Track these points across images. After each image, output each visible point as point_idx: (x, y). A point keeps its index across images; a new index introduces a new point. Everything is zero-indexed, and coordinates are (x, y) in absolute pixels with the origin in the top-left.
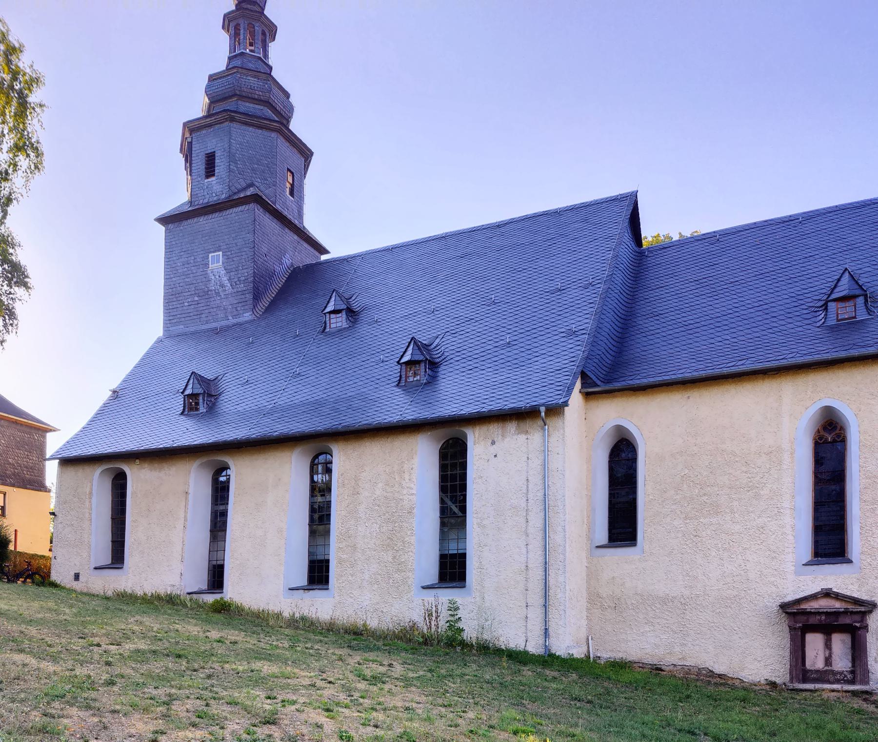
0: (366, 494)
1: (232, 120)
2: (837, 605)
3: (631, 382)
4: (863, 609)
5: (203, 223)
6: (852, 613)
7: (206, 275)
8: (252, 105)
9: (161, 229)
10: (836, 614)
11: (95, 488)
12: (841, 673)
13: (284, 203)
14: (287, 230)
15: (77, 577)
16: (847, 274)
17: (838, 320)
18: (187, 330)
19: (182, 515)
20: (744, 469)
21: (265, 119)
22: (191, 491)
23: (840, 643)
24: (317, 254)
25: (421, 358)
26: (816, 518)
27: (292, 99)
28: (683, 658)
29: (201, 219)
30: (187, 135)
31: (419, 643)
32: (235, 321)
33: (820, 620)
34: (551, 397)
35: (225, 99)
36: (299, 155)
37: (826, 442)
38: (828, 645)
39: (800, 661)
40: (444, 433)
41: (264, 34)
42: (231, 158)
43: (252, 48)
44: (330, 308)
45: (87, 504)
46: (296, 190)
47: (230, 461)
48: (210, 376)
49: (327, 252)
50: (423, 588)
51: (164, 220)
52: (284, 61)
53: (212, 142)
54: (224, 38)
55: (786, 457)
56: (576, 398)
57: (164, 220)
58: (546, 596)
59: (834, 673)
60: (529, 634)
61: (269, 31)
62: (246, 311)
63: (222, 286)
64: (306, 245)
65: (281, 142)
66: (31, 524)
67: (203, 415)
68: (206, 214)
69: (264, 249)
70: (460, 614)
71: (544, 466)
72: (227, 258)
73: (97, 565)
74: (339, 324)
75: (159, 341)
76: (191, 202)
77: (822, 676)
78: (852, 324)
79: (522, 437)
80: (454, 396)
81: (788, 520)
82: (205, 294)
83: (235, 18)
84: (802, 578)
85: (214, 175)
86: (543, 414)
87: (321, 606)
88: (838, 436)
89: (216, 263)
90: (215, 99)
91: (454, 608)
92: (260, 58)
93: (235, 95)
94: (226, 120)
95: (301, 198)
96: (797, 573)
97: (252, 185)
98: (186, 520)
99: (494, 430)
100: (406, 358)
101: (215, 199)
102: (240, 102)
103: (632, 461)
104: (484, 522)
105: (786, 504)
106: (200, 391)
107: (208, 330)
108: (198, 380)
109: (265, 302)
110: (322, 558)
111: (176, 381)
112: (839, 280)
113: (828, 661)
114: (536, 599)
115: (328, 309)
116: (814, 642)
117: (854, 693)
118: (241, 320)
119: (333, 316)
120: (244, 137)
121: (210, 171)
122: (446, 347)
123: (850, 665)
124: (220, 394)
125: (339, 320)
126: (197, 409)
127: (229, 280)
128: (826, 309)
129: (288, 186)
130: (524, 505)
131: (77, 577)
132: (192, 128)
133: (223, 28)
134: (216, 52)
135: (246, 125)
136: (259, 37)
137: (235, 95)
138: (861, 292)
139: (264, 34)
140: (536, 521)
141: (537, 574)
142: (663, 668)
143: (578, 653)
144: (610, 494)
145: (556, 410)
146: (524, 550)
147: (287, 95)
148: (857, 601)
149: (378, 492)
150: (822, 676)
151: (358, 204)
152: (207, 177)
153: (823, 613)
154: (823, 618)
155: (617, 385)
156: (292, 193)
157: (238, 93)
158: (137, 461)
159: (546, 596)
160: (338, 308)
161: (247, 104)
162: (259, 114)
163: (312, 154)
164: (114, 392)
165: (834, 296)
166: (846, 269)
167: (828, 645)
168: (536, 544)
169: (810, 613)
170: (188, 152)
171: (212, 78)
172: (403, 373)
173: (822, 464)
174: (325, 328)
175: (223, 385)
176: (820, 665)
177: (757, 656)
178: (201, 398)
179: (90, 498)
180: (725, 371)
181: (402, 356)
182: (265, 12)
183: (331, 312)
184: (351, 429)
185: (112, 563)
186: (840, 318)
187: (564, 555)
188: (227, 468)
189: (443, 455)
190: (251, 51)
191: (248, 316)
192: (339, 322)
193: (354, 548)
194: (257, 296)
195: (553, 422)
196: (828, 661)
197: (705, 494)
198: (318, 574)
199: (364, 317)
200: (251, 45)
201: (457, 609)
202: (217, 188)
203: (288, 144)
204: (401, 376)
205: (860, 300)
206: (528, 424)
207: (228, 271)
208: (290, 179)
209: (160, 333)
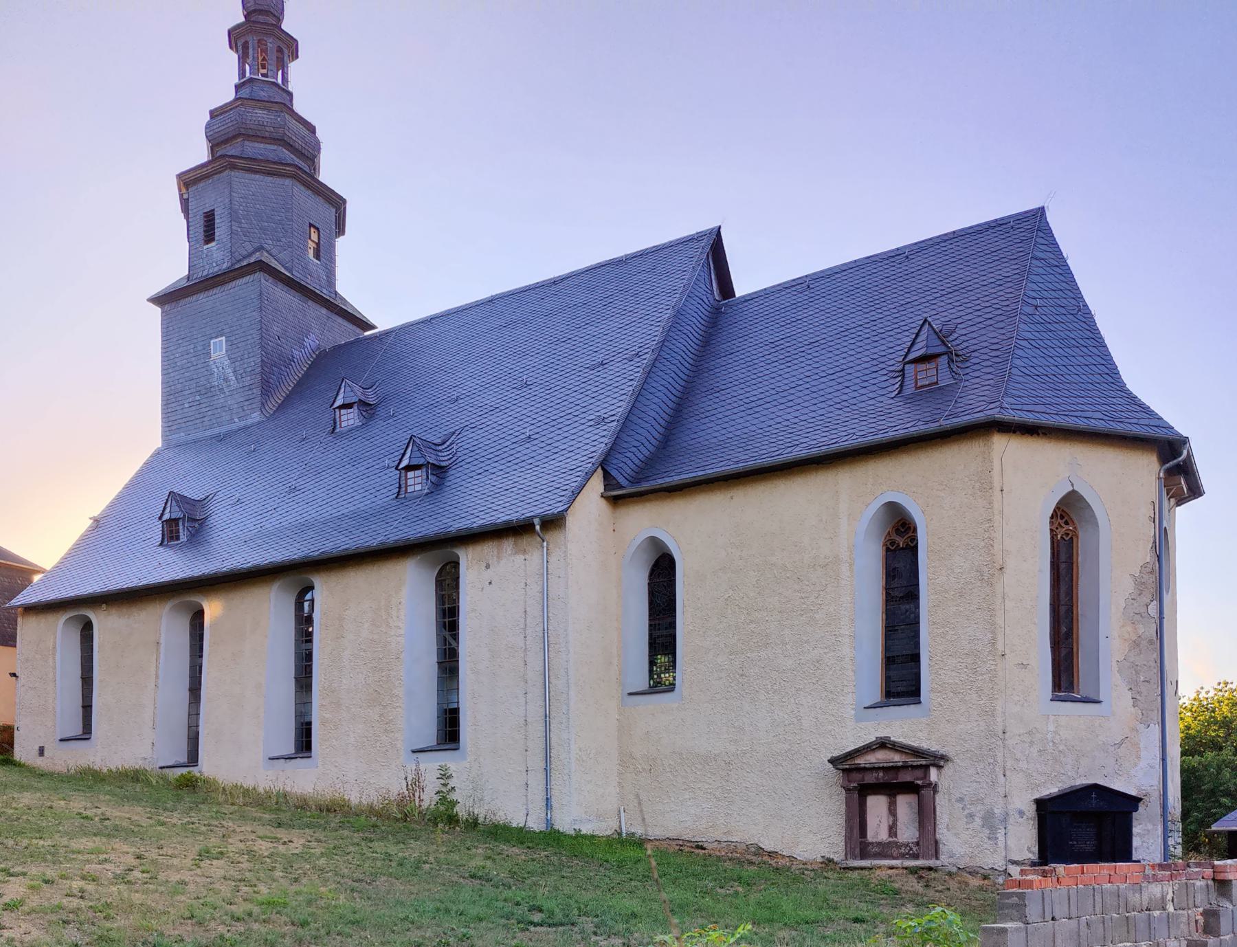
1: (233, 167)
2: (897, 758)
3: (661, 481)
4: (924, 762)
5: (203, 300)
6: (913, 767)
7: (206, 365)
8: (262, 146)
9: (157, 311)
10: (895, 769)
11: (58, 642)
12: (907, 845)
13: (305, 268)
14: (310, 303)
15: (41, 751)
16: (927, 326)
17: (917, 388)
18: (189, 438)
19: (153, 670)
20: (797, 587)
21: (275, 163)
22: (162, 641)
23: (905, 804)
24: (358, 330)
25: (422, 461)
26: (887, 648)
27: (319, 134)
28: (728, 833)
29: (201, 296)
30: (184, 191)
31: (397, 820)
32: (242, 424)
33: (877, 778)
34: (552, 506)
35: (226, 141)
36: (327, 205)
37: (898, 548)
38: (892, 811)
39: (856, 831)
40: (437, 553)
41: (280, 50)
42: (233, 216)
43: (264, 71)
45: (51, 660)
46: (325, 253)
48: (194, 493)
50: (414, 752)
51: (161, 300)
52: (309, 87)
53: (210, 197)
55: (844, 569)
56: (591, 504)
58: (547, 758)
59: (898, 845)
60: (530, 806)
61: (289, 48)
63: (226, 380)
64: (340, 320)
65: (300, 193)
66: (29, 685)
67: (182, 546)
68: (207, 289)
69: (276, 329)
70: (452, 783)
71: (545, 595)
72: (231, 344)
73: (64, 737)
74: (351, 422)
75: (157, 454)
76: (188, 278)
77: (884, 851)
78: (932, 391)
79: (519, 558)
80: (475, 503)
81: (846, 650)
82: (208, 391)
83: (242, 35)
85: (213, 240)
86: (538, 527)
87: (304, 780)
89: (219, 349)
90: (216, 142)
91: (445, 776)
92: (276, 85)
93: (240, 134)
94: (225, 168)
95: (332, 260)
96: (858, 719)
97: (260, 248)
98: (157, 677)
99: (487, 550)
100: (405, 463)
101: (216, 269)
102: (247, 143)
105: (845, 631)
106: (180, 515)
108: (177, 501)
109: (279, 397)
112: (917, 335)
113: (892, 830)
114: (537, 763)
115: (338, 403)
116: (877, 805)
117: (913, 871)
118: (249, 422)
119: (343, 412)
120: (247, 187)
121: (209, 236)
123: (917, 835)
124: (206, 518)
125: (351, 416)
126: (178, 538)
127: (234, 371)
128: (903, 375)
129: (311, 245)
131: (41, 751)
132: (189, 181)
133: (231, 47)
134: (220, 78)
135: (261, 165)
136: (272, 57)
137: (240, 134)
138: (942, 349)
139: (280, 50)
140: (535, 663)
141: (537, 729)
142: (705, 845)
143: (602, 828)
144: (650, 625)
145: (553, 522)
146: (522, 701)
147: (312, 129)
148: (916, 752)
150: (884, 851)
151: (398, 267)
153: (879, 768)
154: (881, 774)
155: (645, 486)
156: (317, 255)
157: (243, 131)
158: (104, 606)
159: (547, 758)
160: (348, 401)
161: (256, 145)
162: (271, 156)
163: (344, 201)
166: (926, 320)
167: (892, 811)
168: (535, 693)
169: (865, 769)
172: (403, 482)
173: (894, 577)
174: (334, 429)
176: (883, 836)
178: (184, 523)
179: (54, 654)
181: (401, 460)
182: (285, 26)
184: (329, 556)
185: (84, 733)
186: (919, 384)
187: (568, 705)
189: (439, 583)
190: (263, 75)
191: (256, 417)
192: (350, 418)
194: (266, 389)
195: (553, 537)
196: (892, 830)
197: (752, 622)
200: (264, 67)
201: (450, 776)
202: (218, 256)
203: (309, 192)
204: (400, 487)
205: (943, 360)
206: (525, 541)
207: (233, 361)
208: (314, 236)
209: (158, 444)
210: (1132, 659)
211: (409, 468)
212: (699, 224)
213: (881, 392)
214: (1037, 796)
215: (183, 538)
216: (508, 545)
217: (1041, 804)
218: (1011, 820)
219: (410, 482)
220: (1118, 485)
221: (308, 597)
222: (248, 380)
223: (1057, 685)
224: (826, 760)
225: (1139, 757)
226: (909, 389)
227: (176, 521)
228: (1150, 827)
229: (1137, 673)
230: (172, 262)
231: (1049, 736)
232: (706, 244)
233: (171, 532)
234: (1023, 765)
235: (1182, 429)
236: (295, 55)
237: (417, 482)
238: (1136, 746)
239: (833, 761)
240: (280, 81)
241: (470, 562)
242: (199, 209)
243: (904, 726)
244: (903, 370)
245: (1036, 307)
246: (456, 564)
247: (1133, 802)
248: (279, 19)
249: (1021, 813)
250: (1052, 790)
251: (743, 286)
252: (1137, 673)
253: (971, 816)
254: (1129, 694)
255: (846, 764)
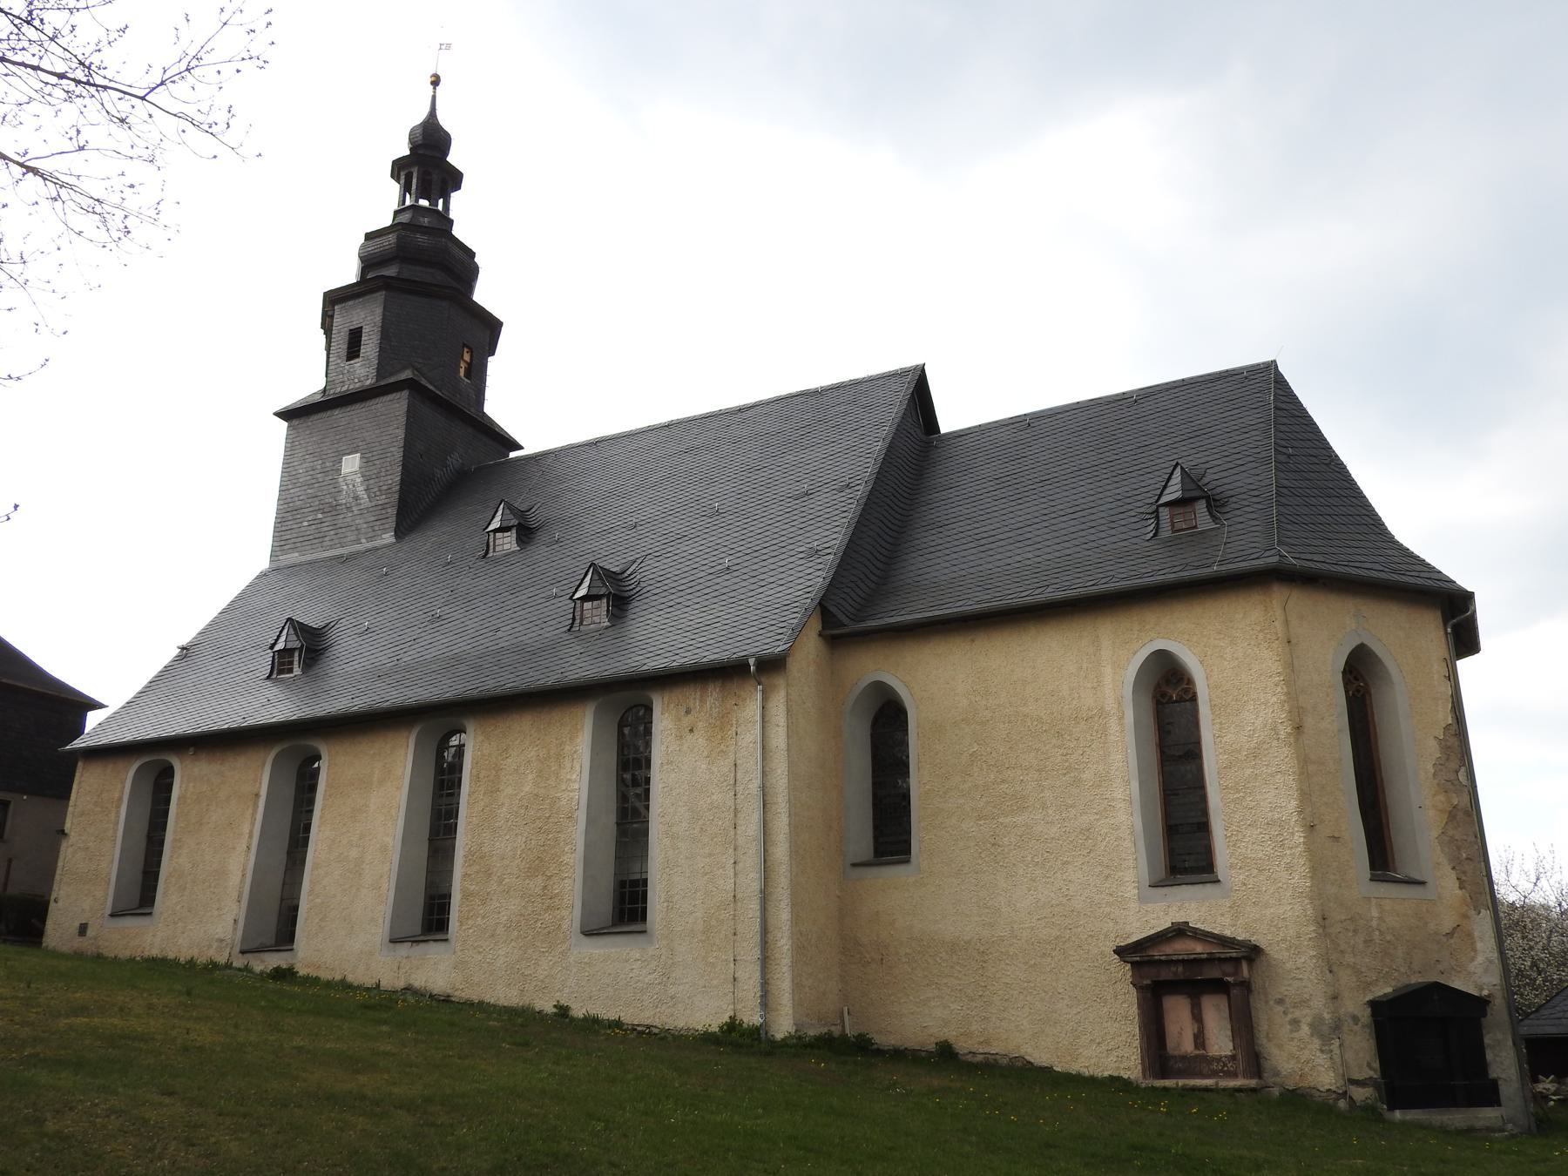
0: (510, 790)
2: (1199, 948)
5: (356, 412)
6: (1220, 959)
9: (283, 425)
10: (1194, 963)
12: (1218, 1059)
15: (83, 930)
18: (303, 559)
25: (603, 591)
28: (987, 1042)
29: (337, 412)
32: (369, 545)
34: (773, 645)
38: (1198, 1017)
44: (495, 524)
45: (113, 815)
46: (477, 375)
47: (324, 749)
48: (313, 620)
49: (520, 447)
51: (285, 415)
52: (468, 217)
54: (395, 188)
57: (285, 415)
61: (453, 179)
62: (385, 531)
63: (356, 498)
72: (366, 461)
75: (263, 575)
76: (324, 390)
80: (657, 640)
82: (333, 509)
84: (1149, 907)
87: (433, 970)
88: (1186, 691)
89: (351, 464)
90: (369, 262)
96: (1142, 899)
99: (691, 696)
100: (582, 592)
103: (1189, 697)
104: (674, 829)
107: (331, 559)
110: (637, 877)
111: (269, 632)
113: (1200, 1039)
116: (1177, 1012)
118: (378, 543)
121: (353, 351)
122: (647, 574)
124: (325, 649)
126: (290, 671)
128: (1157, 517)
130: (730, 803)
132: (334, 300)
134: (382, 203)
144: (874, 784)
149: (527, 789)
152: (349, 358)
153: (1178, 961)
154: (1180, 969)
156: (468, 374)
164: (183, 648)
165: (1164, 499)
167: (1198, 1017)
170: (327, 325)
171: (369, 236)
172: (578, 614)
175: (333, 635)
176: (1188, 1047)
177: (1098, 1035)
178: (305, 649)
180: (1051, 594)
183: (495, 531)
188: (318, 758)
192: (508, 542)
193: (488, 874)
197: (1003, 781)
198: (432, 918)
199: (542, 537)
202: (362, 372)
204: (574, 619)
205: (1201, 506)
207: (366, 478)
208: (467, 357)
210: (1451, 833)
211: (584, 599)
212: (920, 362)
213: (1134, 533)
214: (1370, 997)
215: (297, 671)
216: (770, 937)
217: (1374, 1004)
218: (1345, 1028)
219: (587, 614)
220: (1404, 639)
221: (454, 741)
222: (382, 499)
223: (1374, 865)
224: (1111, 946)
225: (1475, 950)
226: (1166, 532)
227: (292, 651)
228: (1500, 1036)
229: (1459, 848)
230: (307, 374)
231: (1374, 923)
232: (894, 407)
233: (281, 664)
234: (1349, 959)
235: (1464, 582)
236: (457, 187)
237: (598, 614)
238: (1470, 935)
239: (1121, 952)
240: (440, 207)
241: (475, 744)
242: (342, 323)
243: (1192, 907)
244: (1157, 511)
245: (1289, 456)
246: (649, 709)
247: (1479, 1005)
248: (447, 155)
249: (1355, 1019)
250: (1384, 990)
251: (947, 424)
252: (1459, 848)
253: (1295, 1023)
254: (1453, 875)
255: (1137, 955)
